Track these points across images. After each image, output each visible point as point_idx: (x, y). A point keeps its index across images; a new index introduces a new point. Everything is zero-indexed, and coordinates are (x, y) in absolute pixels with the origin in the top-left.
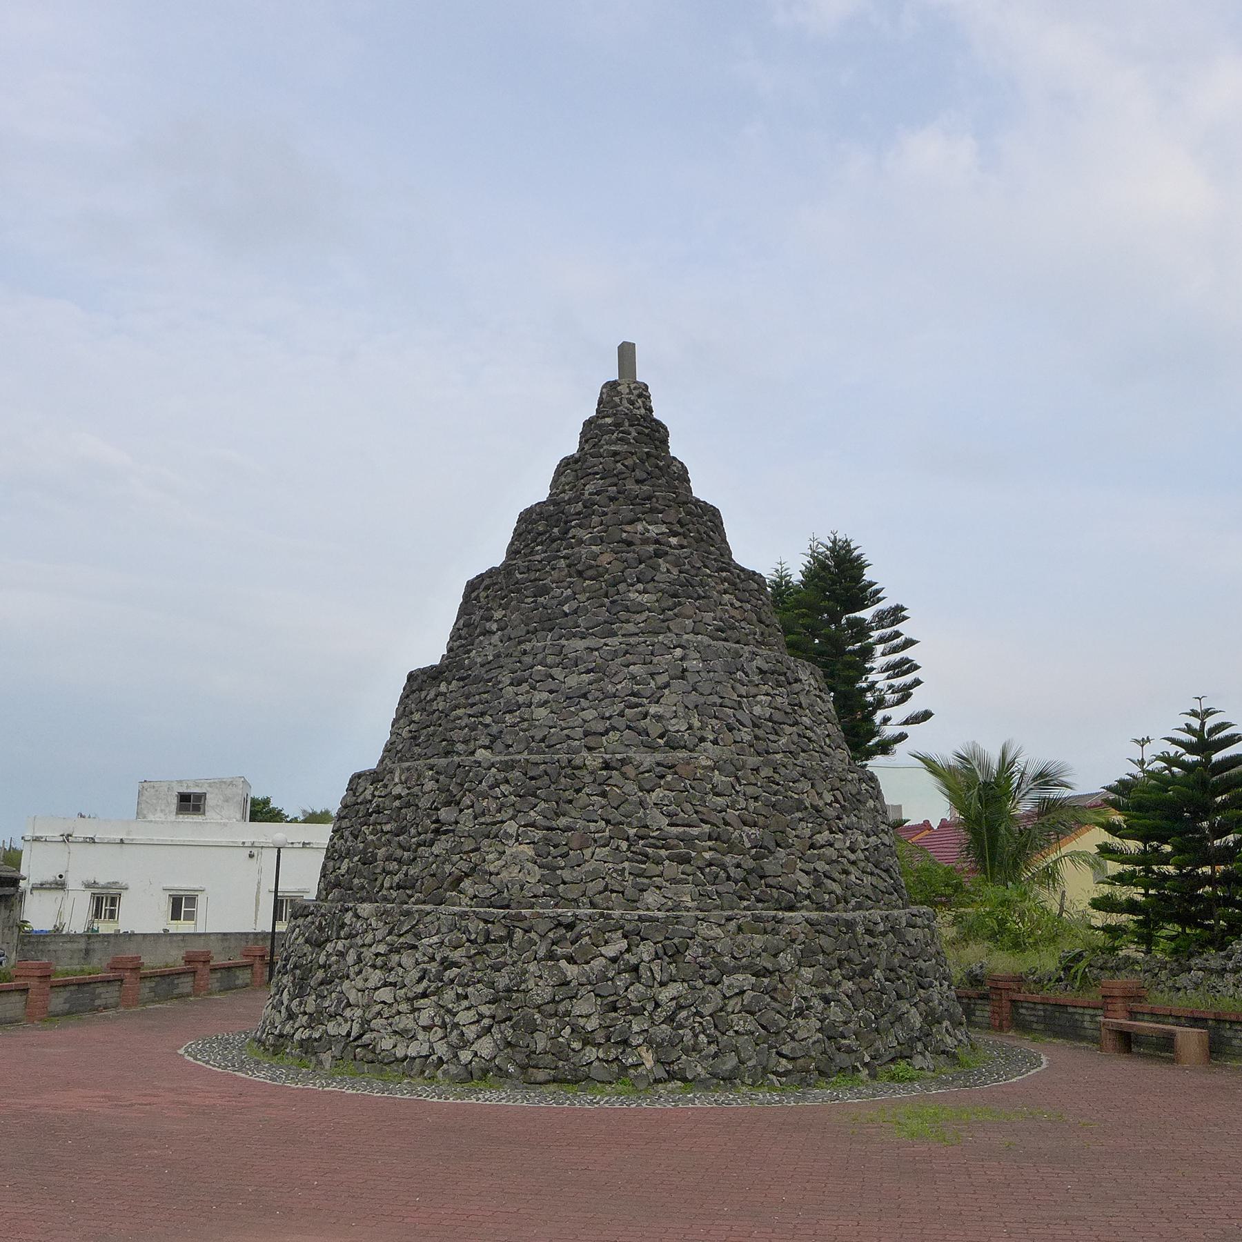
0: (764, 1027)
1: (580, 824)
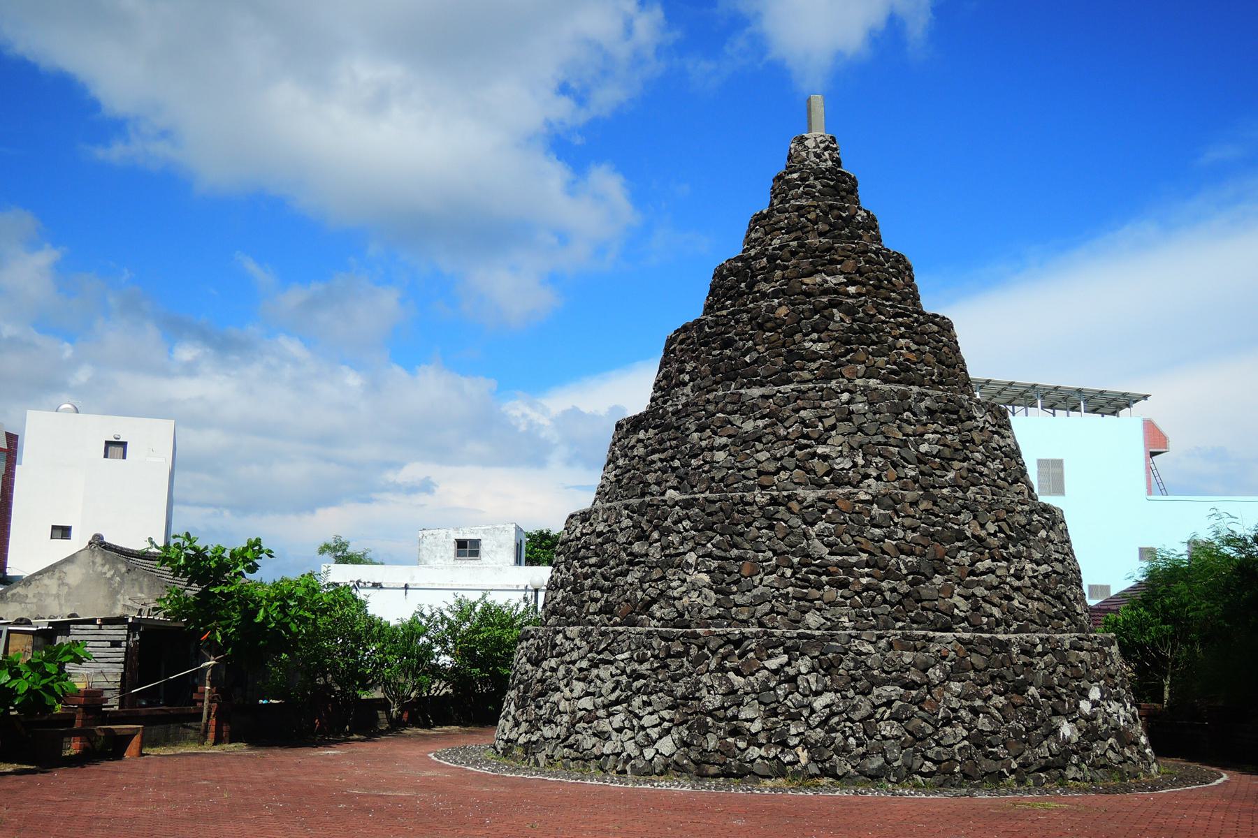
0: (910, 733)
1: (751, 554)
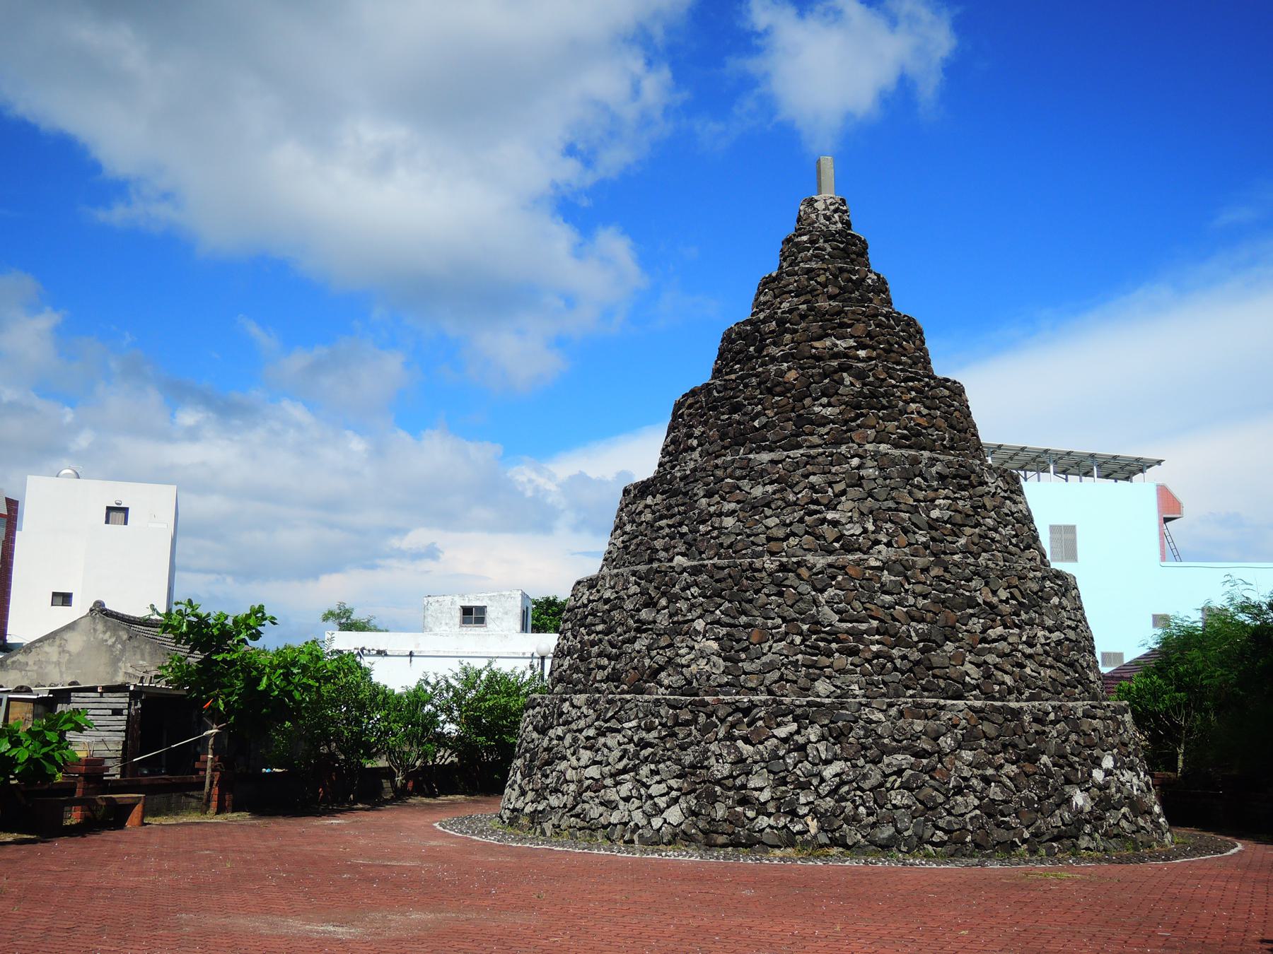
0: (921, 802)
1: (760, 621)
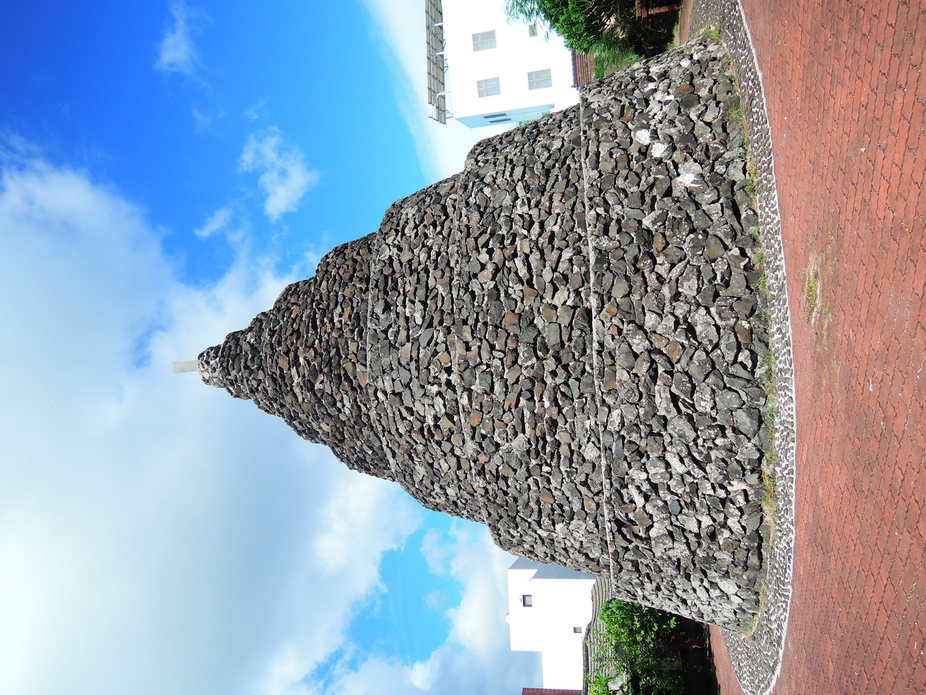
0: (707, 376)
